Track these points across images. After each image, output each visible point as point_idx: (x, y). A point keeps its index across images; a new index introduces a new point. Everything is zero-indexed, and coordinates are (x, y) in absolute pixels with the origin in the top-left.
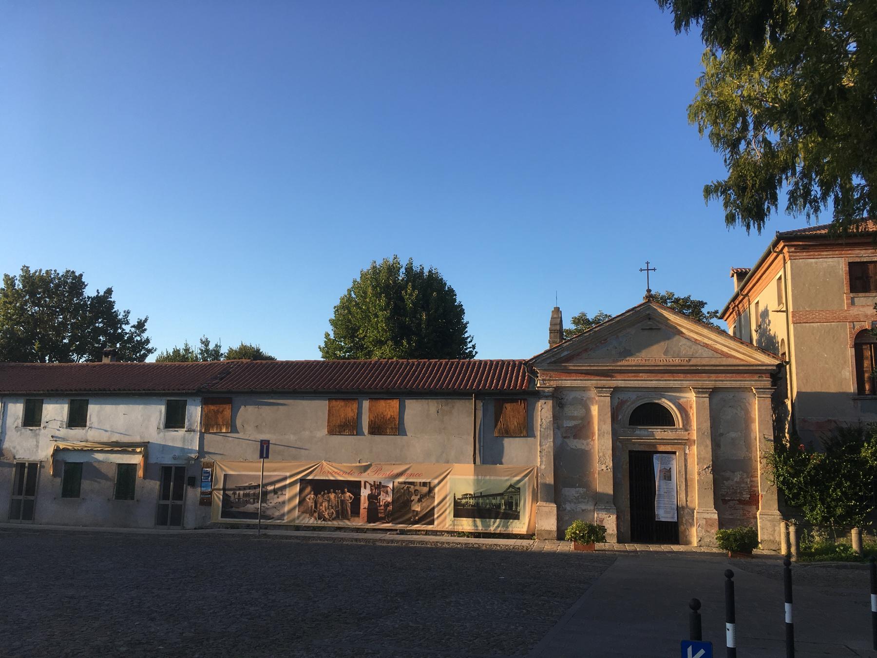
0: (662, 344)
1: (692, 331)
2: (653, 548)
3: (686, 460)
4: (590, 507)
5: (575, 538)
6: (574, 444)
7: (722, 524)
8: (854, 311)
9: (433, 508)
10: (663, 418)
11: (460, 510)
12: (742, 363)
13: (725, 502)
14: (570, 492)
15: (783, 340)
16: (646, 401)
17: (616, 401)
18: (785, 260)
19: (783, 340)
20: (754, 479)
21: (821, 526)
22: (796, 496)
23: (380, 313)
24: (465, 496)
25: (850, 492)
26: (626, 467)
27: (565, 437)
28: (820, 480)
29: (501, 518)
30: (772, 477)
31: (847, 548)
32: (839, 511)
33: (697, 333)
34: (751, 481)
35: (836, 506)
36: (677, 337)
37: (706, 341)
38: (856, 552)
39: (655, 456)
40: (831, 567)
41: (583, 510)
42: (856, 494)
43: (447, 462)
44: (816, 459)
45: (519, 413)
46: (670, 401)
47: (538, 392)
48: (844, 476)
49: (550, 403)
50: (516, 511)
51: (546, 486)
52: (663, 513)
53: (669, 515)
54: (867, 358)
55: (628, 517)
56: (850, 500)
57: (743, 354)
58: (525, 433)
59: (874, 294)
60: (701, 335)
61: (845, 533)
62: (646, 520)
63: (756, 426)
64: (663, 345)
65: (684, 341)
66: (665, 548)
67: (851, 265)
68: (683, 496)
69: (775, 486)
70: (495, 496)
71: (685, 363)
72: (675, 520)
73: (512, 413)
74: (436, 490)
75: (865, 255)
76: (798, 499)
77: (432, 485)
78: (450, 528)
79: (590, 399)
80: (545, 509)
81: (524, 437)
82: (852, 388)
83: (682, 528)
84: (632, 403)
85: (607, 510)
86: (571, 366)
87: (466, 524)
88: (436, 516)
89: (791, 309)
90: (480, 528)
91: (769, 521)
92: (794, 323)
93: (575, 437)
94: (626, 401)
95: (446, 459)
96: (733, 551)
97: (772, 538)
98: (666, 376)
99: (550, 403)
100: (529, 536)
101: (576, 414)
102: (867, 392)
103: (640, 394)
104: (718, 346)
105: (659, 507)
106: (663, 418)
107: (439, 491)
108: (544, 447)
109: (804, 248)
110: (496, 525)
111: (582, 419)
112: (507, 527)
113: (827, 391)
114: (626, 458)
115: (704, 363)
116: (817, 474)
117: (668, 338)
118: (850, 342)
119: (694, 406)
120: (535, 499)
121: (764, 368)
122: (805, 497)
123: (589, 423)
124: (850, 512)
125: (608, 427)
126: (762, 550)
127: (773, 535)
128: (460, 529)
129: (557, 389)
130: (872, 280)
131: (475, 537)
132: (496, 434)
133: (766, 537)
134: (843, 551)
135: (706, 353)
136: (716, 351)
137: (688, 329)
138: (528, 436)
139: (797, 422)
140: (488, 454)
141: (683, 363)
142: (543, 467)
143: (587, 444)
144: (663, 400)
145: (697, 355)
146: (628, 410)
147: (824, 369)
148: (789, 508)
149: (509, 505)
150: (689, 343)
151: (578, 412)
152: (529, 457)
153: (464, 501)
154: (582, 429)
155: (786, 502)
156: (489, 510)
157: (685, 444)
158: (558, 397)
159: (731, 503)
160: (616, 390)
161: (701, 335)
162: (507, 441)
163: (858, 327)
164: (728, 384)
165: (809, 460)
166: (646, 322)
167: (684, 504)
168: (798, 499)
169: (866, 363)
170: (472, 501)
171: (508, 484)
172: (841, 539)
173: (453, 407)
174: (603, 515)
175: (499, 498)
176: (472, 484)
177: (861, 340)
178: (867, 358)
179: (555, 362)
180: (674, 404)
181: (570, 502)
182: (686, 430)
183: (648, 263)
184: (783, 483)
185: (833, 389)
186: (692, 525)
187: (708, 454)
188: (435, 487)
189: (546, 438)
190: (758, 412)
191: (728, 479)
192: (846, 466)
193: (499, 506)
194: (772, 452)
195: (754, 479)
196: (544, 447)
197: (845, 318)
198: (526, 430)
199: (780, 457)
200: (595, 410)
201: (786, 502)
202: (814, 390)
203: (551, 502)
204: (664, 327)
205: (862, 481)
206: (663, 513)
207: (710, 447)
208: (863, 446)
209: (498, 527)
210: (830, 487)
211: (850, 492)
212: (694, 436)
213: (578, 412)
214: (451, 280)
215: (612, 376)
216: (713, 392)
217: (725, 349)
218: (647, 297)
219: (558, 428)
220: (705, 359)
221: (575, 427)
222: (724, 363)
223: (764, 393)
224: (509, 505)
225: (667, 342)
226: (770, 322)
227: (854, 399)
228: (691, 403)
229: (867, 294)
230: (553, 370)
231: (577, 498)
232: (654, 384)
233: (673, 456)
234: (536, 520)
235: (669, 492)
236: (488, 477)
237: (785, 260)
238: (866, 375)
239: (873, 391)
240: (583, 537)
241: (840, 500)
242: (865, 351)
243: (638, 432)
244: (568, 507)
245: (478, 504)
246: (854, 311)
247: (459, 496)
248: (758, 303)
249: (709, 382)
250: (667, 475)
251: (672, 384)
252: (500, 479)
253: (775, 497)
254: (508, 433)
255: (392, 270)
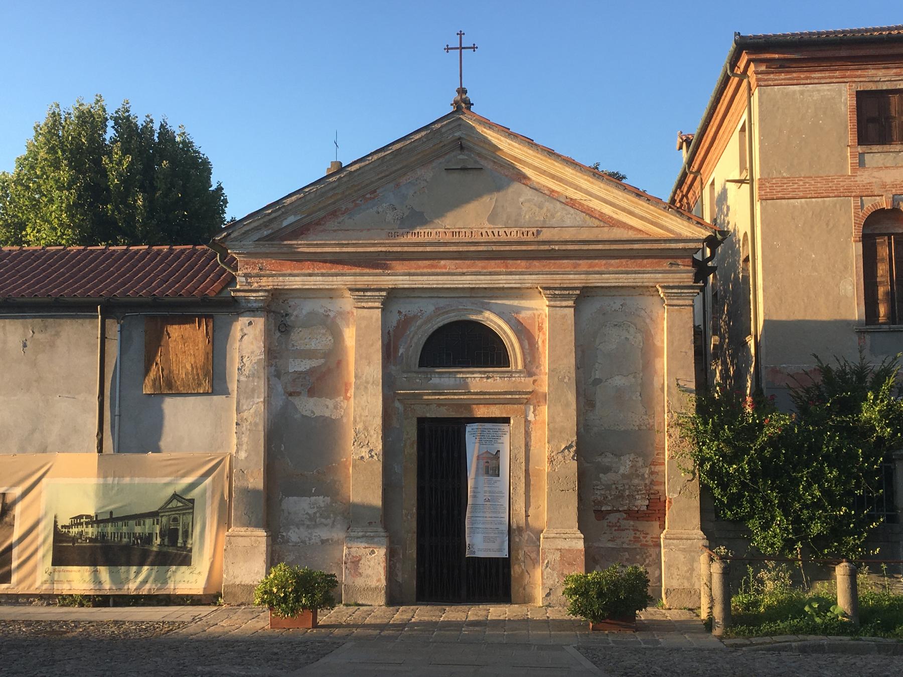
0: (486, 199)
1: (544, 172)
2: (454, 614)
3: (527, 434)
4: (338, 534)
5: (270, 603)
6: (308, 406)
7: (592, 559)
8: (864, 177)
9: (10, 548)
10: (484, 349)
11: (66, 551)
12: (640, 236)
13: (601, 515)
14: (299, 506)
15: (746, 234)
16: (453, 317)
17: (394, 319)
18: (750, 89)
19: (746, 234)
20: (657, 468)
21: (779, 558)
22: (735, 500)
23: (56, 194)
24: (77, 520)
25: (838, 490)
26: (411, 450)
27: (291, 394)
28: (780, 467)
29: (152, 564)
30: (690, 464)
31: (827, 604)
32: (816, 528)
33: (553, 177)
34: (652, 473)
35: (811, 519)
36: (516, 186)
37: (572, 193)
38: (844, 615)
39: (469, 428)
40: (791, 648)
41: (323, 542)
42: (850, 493)
43: (44, 451)
44: (776, 424)
45: (195, 344)
46: (500, 315)
47: (235, 300)
48: (827, 457)
49: (260, 323)
50: (184, 547)
51: (248, 492)
52: (482, 542)
53: (495, 546)
54: (883, 260)
55: (413, 551)
56: (836, 505)
57: (642, 218)
58: (206, 386)
59: (898, 148)
60: (560, 180)
61: (826, 574)
62: (445, 559)
63: (663, 364)
64: (487, 202)
65: (528, 194)
66: (475, 612)
67: (862, 96)
68: (519, 505)
69: (696, 481)
70: (139, 518)
71: (530, 238)
72: (505, 554)
73: (185, 343)
74: (18, 509)
75: (883, 78)
76: (740, 506)
77: (9, 499)
78: (44, 589)
79: (341, 314)
80: (242, 542)
81: (206, 394)
82: (856, 312)
83: (516, 570)
84: (425, 323)
85: (368, 539)
86: (303, 246)
87: (78, 579)
88: (14, 564)
89: (757, 175)
90: (108, 586)
91: (684, 550)
92: (761, 199)
93: (312, 392)
94: (415, 317)
95: (38, 442)
96: (594, 617)
97: (686, 585)
98: (493, 265)
99: (260, 323)
100: (210, 598)
101: (313, 345)
102: (882, 319)
103: (442, 303)
104: (595, 204)
105: (474, 530)
106: (484, 349)
107: (22, 513)
108: (245, 415)
109: (783, 66)
110: (141, 578)
111: (327, 355)
112: (165, 582)
113: (814, 318)
114: (411, 433)
115: (567, 237)
116: (776, 455)
117: (498, 187)
118: (855, 232)
119: (546, 326)
120: (224, 521)
121: (680, 245)
122: (752, 502)
123: (339, 363)
124: (837, 530)
125: (375, 371)
126: (666, 610)
127: (689, 579)
128: (64, 589)
129: (277, 296)
130: (895, 123)
131: (96, 605)
132: (147, 390)
133: (675, 584)
134: (818, 613)
135: (571, 217)
136: (589, 212)
137: (535, 168)
138: (213, 393)
139: (763, 373)
140: (129, 427)
141: (525, 238)
142: (243, 455)
143: (336, 407)
144: (487, 314)
145: (553, 222)
146: (417, 337)
147: (809, 282)
148: (723, 524)
149: (170, 535)
150: (537, 198)
151: (319, 341)
152: (213, 434)
153: (74, 531)
154: (323, 379)
155: (717, 511)
156: (127, 548)
157: (528, 402)
158: (278, 311)
159: (613, 518)
160: (392, 296)
161: (560, 180)
162: (169, 404)
163: (870, 205)
164: (610, 280)
165: (761, 426)
166: (450, 155)
167: (522, 523)
168: (740, 506)
169: (882, 269)
170: (91, 531)
171: (170, 492)
172: (818, 585)
173: (57, 334)
174: (359, 549)
175: (149, 522)
176: (92, 494)
177: (875, 227)
178: (883, 260)
179: (269, 238)
180: (508, 322)
181: (298, 526)
182: (530, 374)
183: (461, 34)
184: (711, 474)
185: (825, 315)
186: (535, 562)
187: (569, 421)
188: (15, 503)
189: (251, 394)
190: (668, 334)
191: (607, 470)
192: (832, 438)
193: (148, 539)
194: (692, 413)
195: (657, 468)
196: (245, 415)
197: (848, 189)
198: (213, 378)
199: (705, 423)
200: (350, 336)
201: (717, 511)
202: (792, 318)
203: (257, 526)
204: (488, 165)
205: (861, 469)
206: (482, 542)
207: (574, 406)
208: (866, 399)
209: (145, 582)
210: (798, 481)
211: (838, 490)
212: (544, 387)
213: (319, 341)
214: (205, 145)
215: (386, 267)
216: (583, 296)
217: (607, 210)
218: (456, 102)
219: (278, 375)
220: (567, 228)
221: (311, 371)
222: (605, 237)
223: (679, 296)
224: (170, 535)
225: (495, 196)
226: (728, 208)
227: (861, 332)
228: (538, 319)
229: (887, 148)
230: (266, 255)
231: (312, 518)
232: (467, 281)
233: (505, 427)
234: (228, 562)
235: (493, 499)
236: (127, 480)
237: (750, 89)
238: (881, 290)
239: (892, 317)
240: (285, 599)
241: (817, 505)
242: (879, 249)
243: (435, 380)
244: (294, 535)
245: (103, 536)
246: (864, 177)
247: (64, 520)
248: (713, 184)
249: (575, 276)
250: (492, 467)
251: (503, 281)
252: (153, 481)
253: (696, 503)
254: (169, 387)
255: (90, 121)
